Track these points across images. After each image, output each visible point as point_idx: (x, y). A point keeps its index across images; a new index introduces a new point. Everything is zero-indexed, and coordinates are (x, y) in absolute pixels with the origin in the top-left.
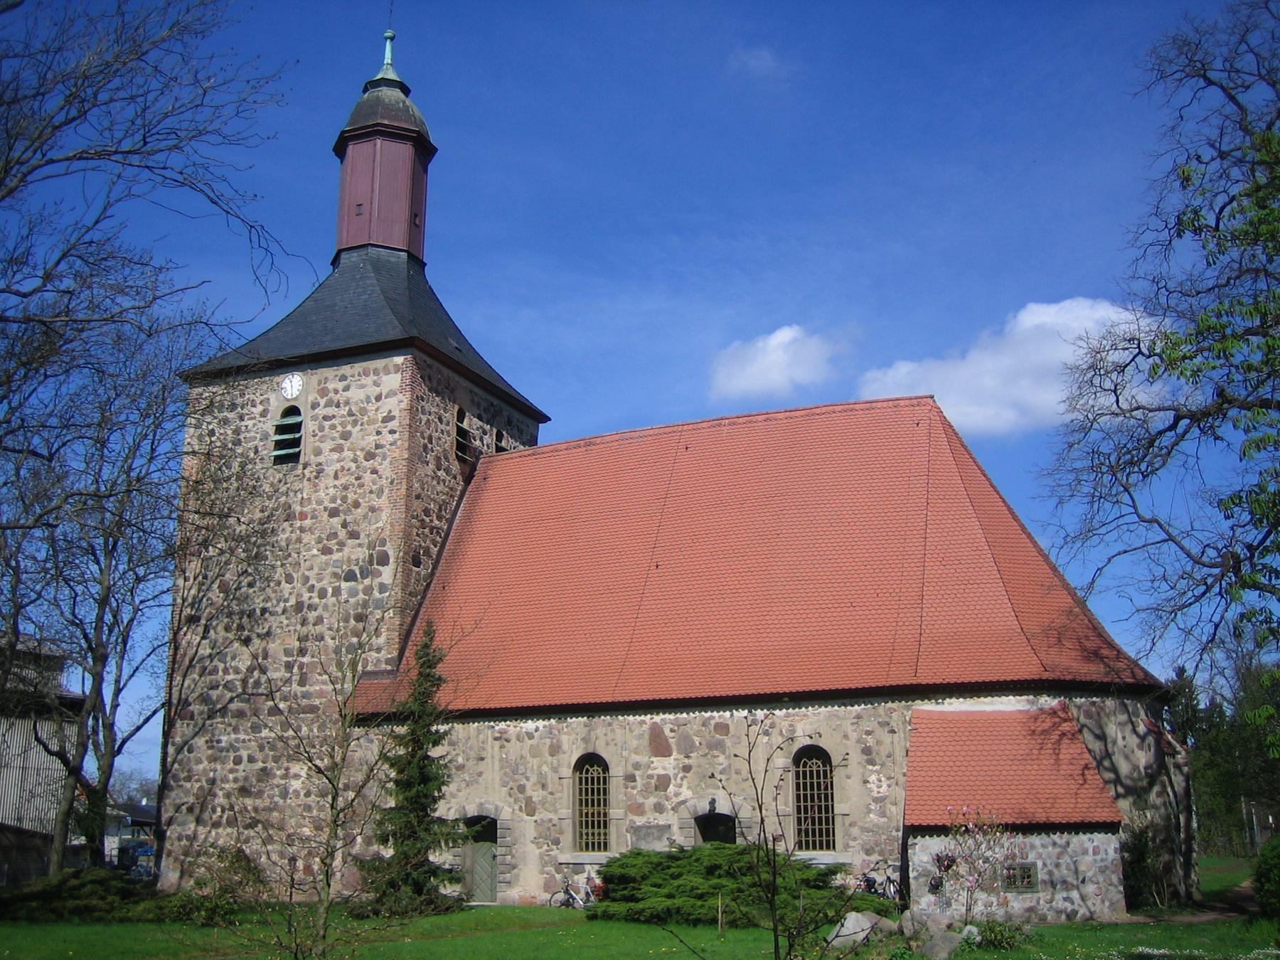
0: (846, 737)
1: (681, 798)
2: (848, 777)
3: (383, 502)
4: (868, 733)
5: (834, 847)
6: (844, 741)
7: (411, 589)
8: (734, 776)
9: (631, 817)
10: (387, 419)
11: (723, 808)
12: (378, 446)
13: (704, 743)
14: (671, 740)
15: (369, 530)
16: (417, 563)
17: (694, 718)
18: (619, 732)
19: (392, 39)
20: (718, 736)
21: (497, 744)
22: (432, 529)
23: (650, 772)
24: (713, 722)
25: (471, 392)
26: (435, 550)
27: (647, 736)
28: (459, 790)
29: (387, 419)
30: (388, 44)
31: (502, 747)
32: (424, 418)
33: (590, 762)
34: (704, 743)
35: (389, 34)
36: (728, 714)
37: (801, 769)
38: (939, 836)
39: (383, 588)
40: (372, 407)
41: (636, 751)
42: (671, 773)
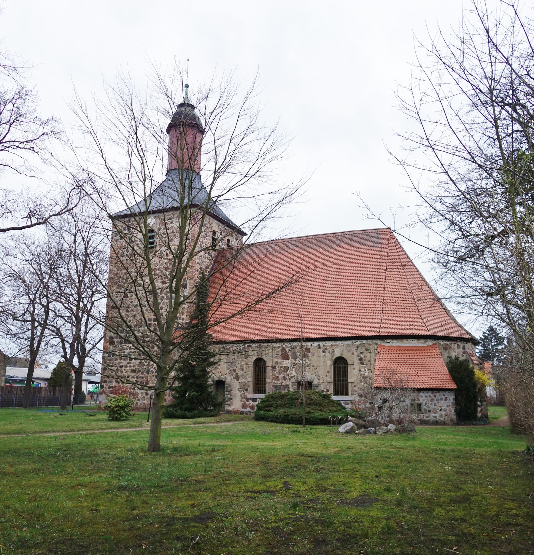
4: (362, 353)
41: (276, 358)
42: (289, 366)
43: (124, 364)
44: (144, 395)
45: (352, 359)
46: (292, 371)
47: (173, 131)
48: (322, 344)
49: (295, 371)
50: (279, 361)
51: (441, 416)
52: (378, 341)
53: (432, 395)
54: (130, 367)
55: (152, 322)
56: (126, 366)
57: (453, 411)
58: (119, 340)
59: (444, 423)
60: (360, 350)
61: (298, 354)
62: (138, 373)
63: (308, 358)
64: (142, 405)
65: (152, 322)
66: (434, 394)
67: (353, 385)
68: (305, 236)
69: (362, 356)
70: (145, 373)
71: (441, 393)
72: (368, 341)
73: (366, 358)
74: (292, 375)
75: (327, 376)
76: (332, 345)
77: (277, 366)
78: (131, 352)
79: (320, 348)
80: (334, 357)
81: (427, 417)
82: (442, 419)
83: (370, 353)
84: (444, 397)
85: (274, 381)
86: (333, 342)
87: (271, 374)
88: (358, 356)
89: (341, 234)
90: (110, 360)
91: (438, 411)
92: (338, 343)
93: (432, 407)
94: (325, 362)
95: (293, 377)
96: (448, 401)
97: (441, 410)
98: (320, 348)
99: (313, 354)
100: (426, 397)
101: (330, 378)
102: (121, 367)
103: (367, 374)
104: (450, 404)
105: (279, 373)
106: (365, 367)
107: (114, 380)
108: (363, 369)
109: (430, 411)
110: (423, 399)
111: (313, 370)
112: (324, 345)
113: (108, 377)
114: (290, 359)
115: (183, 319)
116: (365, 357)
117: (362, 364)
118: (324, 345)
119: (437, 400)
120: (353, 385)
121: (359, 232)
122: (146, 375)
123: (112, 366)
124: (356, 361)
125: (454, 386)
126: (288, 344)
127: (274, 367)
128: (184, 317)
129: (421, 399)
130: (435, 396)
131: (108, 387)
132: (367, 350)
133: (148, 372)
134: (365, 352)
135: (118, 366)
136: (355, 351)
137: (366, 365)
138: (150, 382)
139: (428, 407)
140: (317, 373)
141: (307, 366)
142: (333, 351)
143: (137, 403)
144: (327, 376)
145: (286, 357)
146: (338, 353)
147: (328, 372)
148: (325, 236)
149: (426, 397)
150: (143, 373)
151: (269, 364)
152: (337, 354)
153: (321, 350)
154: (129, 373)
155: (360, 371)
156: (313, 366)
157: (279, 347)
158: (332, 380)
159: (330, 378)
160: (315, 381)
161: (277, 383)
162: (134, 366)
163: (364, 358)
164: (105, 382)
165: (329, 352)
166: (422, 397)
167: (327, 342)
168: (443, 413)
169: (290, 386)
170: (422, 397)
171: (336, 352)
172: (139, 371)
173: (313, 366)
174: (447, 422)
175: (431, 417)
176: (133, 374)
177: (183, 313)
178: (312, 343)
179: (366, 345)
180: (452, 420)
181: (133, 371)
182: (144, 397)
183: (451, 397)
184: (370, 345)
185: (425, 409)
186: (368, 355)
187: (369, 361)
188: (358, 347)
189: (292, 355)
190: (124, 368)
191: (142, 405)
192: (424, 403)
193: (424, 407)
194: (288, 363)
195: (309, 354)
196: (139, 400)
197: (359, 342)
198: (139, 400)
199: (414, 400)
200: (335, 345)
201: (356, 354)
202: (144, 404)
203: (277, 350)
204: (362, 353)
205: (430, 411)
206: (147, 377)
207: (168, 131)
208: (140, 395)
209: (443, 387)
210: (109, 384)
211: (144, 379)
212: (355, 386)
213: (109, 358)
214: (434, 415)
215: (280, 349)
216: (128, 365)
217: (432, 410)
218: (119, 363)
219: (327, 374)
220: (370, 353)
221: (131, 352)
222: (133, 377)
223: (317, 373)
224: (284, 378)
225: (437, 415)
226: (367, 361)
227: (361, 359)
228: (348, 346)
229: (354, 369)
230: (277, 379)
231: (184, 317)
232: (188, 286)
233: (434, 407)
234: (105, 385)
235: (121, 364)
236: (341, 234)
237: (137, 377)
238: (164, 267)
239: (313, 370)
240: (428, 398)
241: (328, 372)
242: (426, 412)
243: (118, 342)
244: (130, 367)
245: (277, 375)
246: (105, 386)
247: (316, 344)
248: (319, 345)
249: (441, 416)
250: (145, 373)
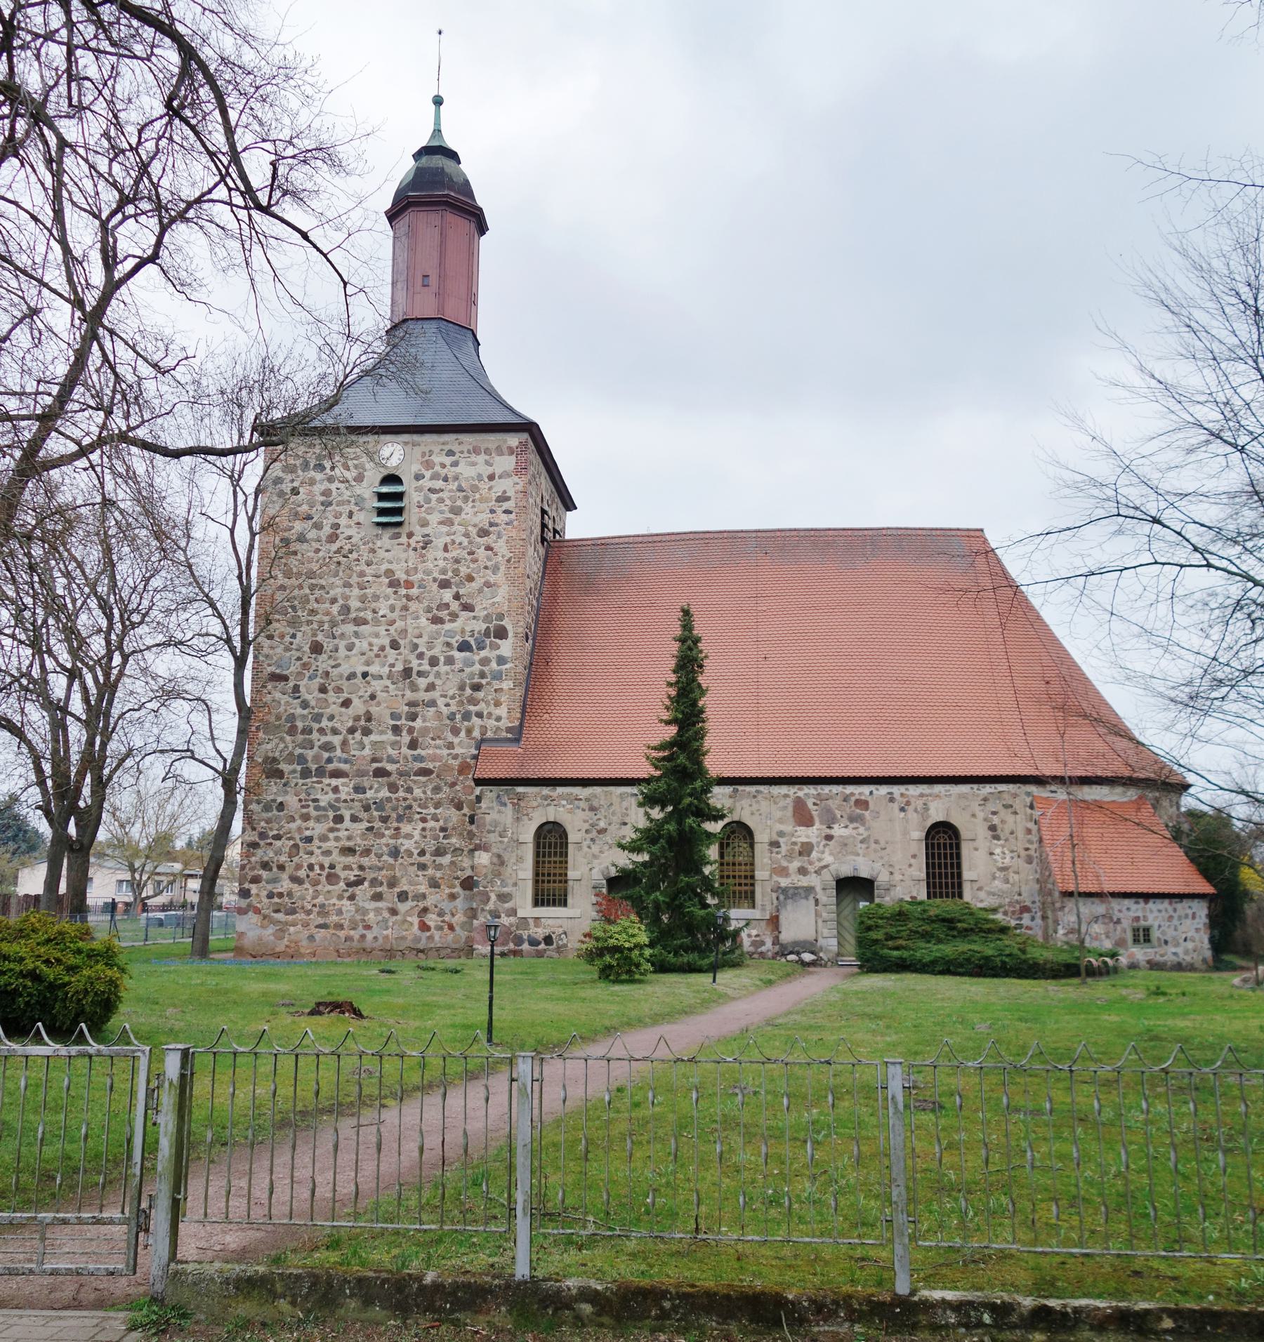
4: (994, 813)
41: (781, 821)
42: (814, 841)
43: (316, 833)
44: (386, 914)
45: (972, 828)
46: (823, 852)
47: (404, 221)
48: (897, 790)
49: (831, 854)
50: (788, 828)
51: (1186, 952)
52: (1033, 789)
53: (1170, 909)
54: (337, 839)
55: (403, 721)
56: (324, 838)
57: (1206, 941)
58: (299, 768)
59: (1191, 968)
60: (991, 807)
61: (838, 813)
62: (361, 855)
63: (863, 824)
64: (381, 940)
65: (403, 721)
66: (1175, 905)
67: (976, 886)
68: (779, 530)
69: (996, 820)
70: (385, 858)
71: (1186, 903)
72: (1011, 786)
73: (1006, 826)
74: (823, 863)
75: (910, 865)
76: (922, 795)
77: (781, 840)
78: (337, 800)
79: (892, 800)
80: (929, 823)
81: (1162, 956)
82: (1188, 958)
83: (1016, 813)
84: (1190, 912)
85: (775, 878)
86: (925, 786)
87: (766, 860)
88: (985, 820)
89: (870, 533)
90: (268, 821)
91: (1181, 941)
92: (939, 788)
93: (1170, 934)
94: (905, 833)
95: (826, 867)
96: (1197, 920)
97: (1185, 940)
98: (892, 800)
99: (877, 815)
100: (1160, 911)
101: (919, 870)
102: (309, 840)
103: (1007, 861)
104: (1201, 926)
105: (789, 857)
106: (1003, 846)
107: (285, 876)
108: (998, 851)
109: (1166, 942)
110: (1154, 914)
111: (875, 851)
112: (902, 795)
113: (265, 866)
114: (817, 825)
115: (499, 719)
116: (1003, 822)
117: (997, 838)
118: (902, 795)
119: (1180, 918)
120: (976, 886)
121: (914, 532)
122: (391, 861)
123: (278, 837)
124: (982, 832)
125: (1208, 889)
126: (810, 790)
127: (775, 844)
128: (502, 711)
129: (1151, 917)
130: (1175, 910)
131: (265, 893)
132: (1007, 806)
133: (395, 853)
134: (1003, 812)
135: (297, 837)
136: (977, 810)
137: (1006, 840)
138: (404, 881)
139: (1164, 933)
140: (886, 858)
141: (862, 842)
142: (926, 808)
143: (363, 937)
144: (910, 865)
145: (806, 821)
146: (937, 814)
147: (914, 856)
148: (831, 533)
149: (1160, 911)
150: (379, 856)
151: (761, 837)
152: (936, 815)
153: (896, 806)
154: (336, 857)
155: (992, 854)
156: (876, 842)
157: (786, 796)
158: (924, 875)
159: (920, 870)
160: (882, 878)
161: (784, 882)
162: (349, 838)
163: (999, 826)
164: (256, 880)
165: (916, 810)
166: (1151, 911)
167: (911, 787)
168: (1190, 945)
169: (818, 889)
170: (1151, 911)
171: (932, 811)
172: (367, 852)
173: (876, 842)
174: (1197, 965)
175: (1169, 954)
176: (350, 860)
177: (497, 704)
178: (872, 788)
179: (1005, 796)
180: (1204, 960)
181: (349, 851)
182: (385, 921)
183: (1201, 910)
184: (1015, 796)
185: (1159, 939)
186: (1010, 819)
187: (1012, 833)
188: (985, 799)
189: (820, 816)
190: (316, 842)
191: (381, 940)
192: (1156, 924)
193: (1155, 934)
194: (811, 834)
195: (867, 813)
196: (368, 927)
197: (988, 789)
198: (368, 927)
199: (1137, 919)
200: (930, 795)
201: (981, 815)
202: (386, 937)
203: (782, 804)
204: (994, 813)
205: (1166, 942)
206: (392, 867)
207: (393, 215)
208: (372, 915)
209: (1187, 890)
210: (269, 887)
211: (384, 872)
212: (980, 889)
213: (265, 815)
214: (1174, 950)
215: (789, 800)
216: (331, 835)
217: (1169, 939)
218: (299, 829)
219: (913, 861)
220: (1016, 813)
221: (337, 800)
222: (347, 868)
223: (886, 858)
224: (802, 871)
225: (1179, 950)
226: (1007, 831)
227: (993, 828)
228: (962, 796)
229: (976, 849)
230: (783, 872)
231: (502, 711)
232: (510, 634)
233: (1174, 933)
234: (254, 889)
235: (308, 833)
236: (870, 533)
237: (361, 868)
238: (435, 580)
239: (875, 851)
240: (1164, 913)
241: (914, 856)
242: (1160, 946)
243: (294, 771)
244: (337, 839)
245: (785, 864)
246: (254, 891)
247: (883, 790)
248: (890, 793)
249: (1186, 952)
250: (385, 858)
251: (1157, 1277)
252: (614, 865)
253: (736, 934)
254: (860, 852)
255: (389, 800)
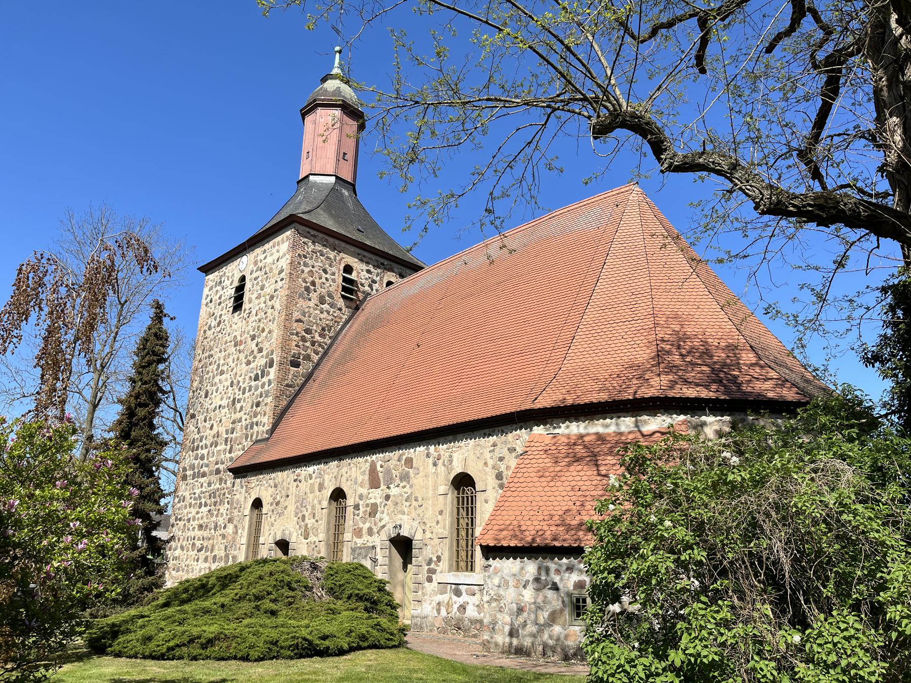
0: (486, 464)
1: (383, 523)
2: (486, 502)
3: (274, 326)
4: (501, 459)
5: (472, 570)
6: (485, 468)
7: (289, 382)
8: (414, 503)
9: (355, 539)
10: (281, 272)
11: (405, 532)
12: (276, 290)
13: (398, 475)
14: (380, 474)
15: (266, 346)
16: (295, 364)
17: (393, 456)
18: (354, 469)
19: (340, 52)
20: (406, 469)
21: (295, 484)
22: (313, 343)
23: (368, 502)
24: (404, 457)
25: (359, 254)
26: (315, 358)
27: (367, 472)
28: (275, 521)
29: (281, 272)
30: (338, 55)
31: (297, 486)
32: (306, 270)
33: (338, 495)
34: (398, 475)
35: (337, 48)
36: (412, 450)
37: (461, 495)
38: (515, 558)
39: (270, 382)
40: (274, 267)
41: (362, 485)
42: (378, 501)
88: (494, 467)
94: (435, 488)
98: (428, 456)
124: (492, 482)
152: (458, 469)
153: (431, 460)
156: (416, 500)
241: (441, 513)
251: (596, 25)
252: (172, 538)
253: (38, 671)
254: (406, 510)
255: (739, 496)
